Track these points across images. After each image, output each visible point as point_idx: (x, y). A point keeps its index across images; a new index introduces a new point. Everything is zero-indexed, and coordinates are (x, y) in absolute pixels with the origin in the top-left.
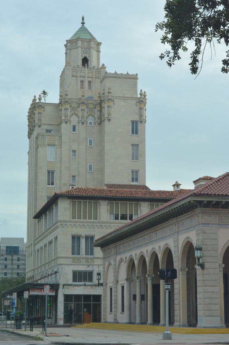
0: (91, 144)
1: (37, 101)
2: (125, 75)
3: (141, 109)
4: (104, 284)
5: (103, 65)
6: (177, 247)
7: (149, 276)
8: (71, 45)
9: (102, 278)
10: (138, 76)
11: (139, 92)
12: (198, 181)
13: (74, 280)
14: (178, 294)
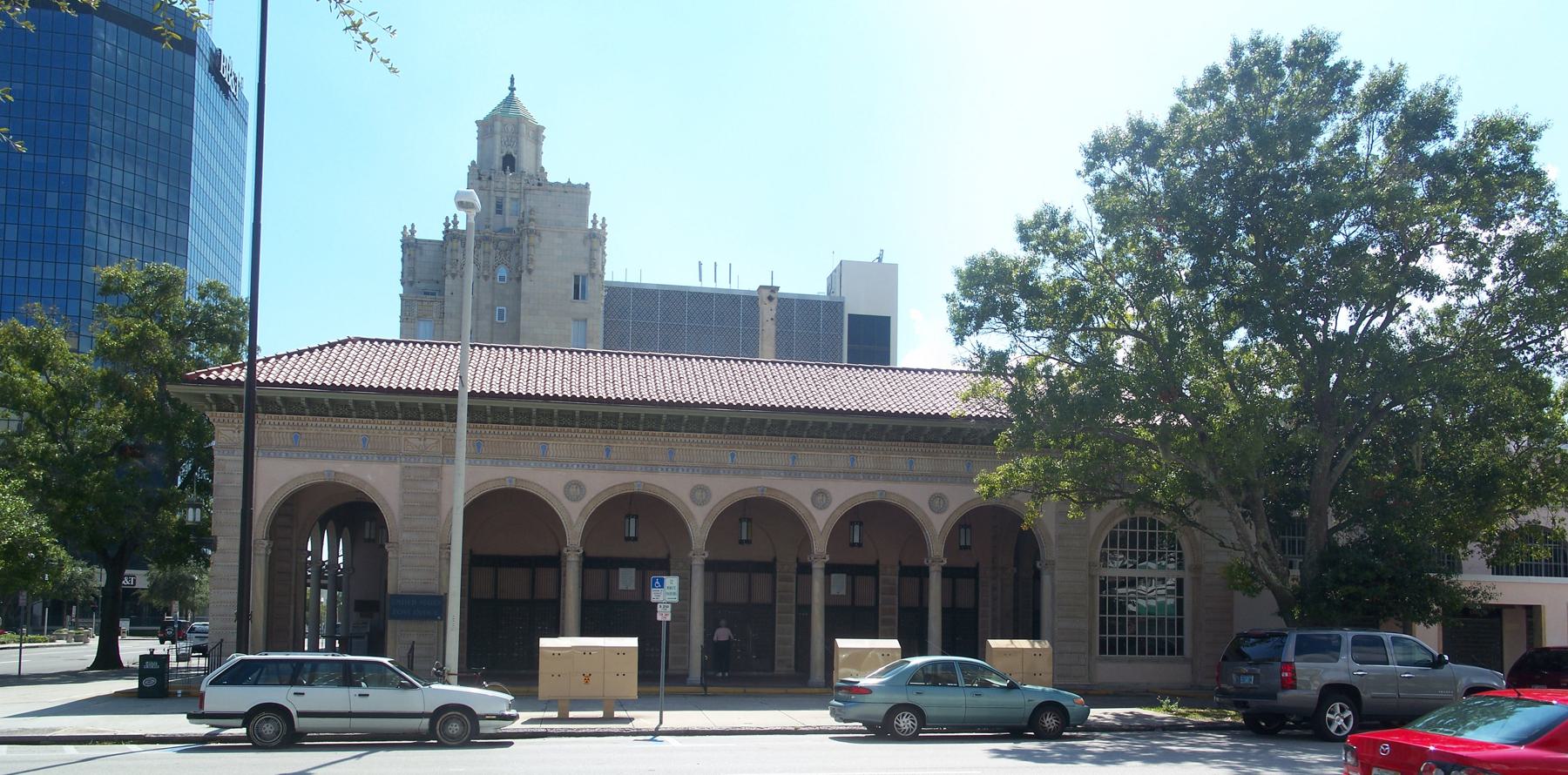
0: (501, 318)
3: (592, 250)
6: (112, 553)
8: (486, 128)
11: (591, 218)
12: (356, 428)
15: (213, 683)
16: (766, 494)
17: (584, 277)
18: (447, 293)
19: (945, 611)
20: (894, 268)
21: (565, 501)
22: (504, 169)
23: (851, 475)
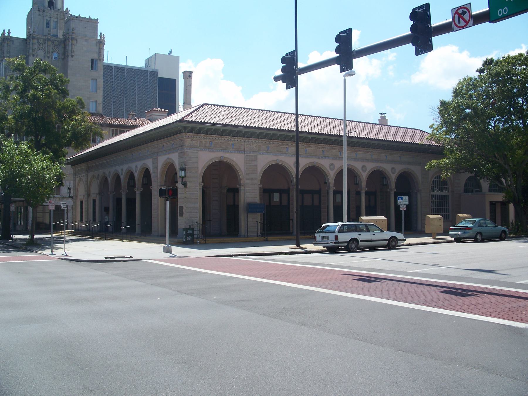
1: (6, 34)
2: (87, 19)
4: (74, 197)
7: (430, 165)
9: (72, 192)
10: (99, 21)
11: (99, 34)
12: (232, 140)
19: (366, 207)
20: (178, 58)
23: (372, 161)
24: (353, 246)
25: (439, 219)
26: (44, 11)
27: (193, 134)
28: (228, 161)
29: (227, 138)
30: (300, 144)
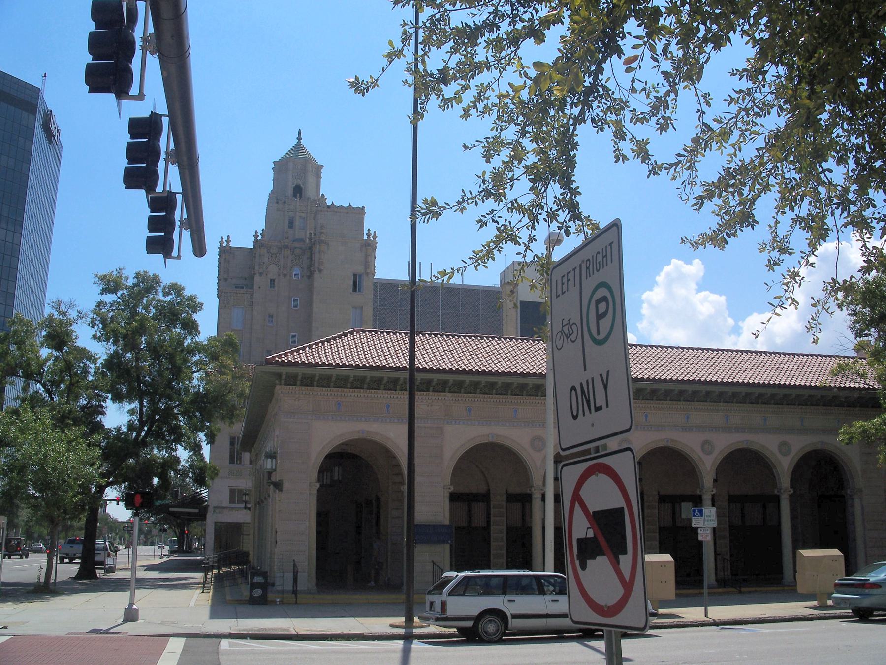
1: (225, 245)
3: (367, 256)
5: (323, 195)
8: (280, 167)
11: (366, 232)
13: (232, 501)
14: (470, 522)
15: (451, 593)
16: (670, 445)
17: (360, 276)
18: (256, 287)
21: (779, 456)
22: (295, 196)
24: (491, 628)
25: (834, 558)
26: (285, 203)
27: (297, 388)
28: (377, 439)
29: (373, 393)
30: (418, 396)
